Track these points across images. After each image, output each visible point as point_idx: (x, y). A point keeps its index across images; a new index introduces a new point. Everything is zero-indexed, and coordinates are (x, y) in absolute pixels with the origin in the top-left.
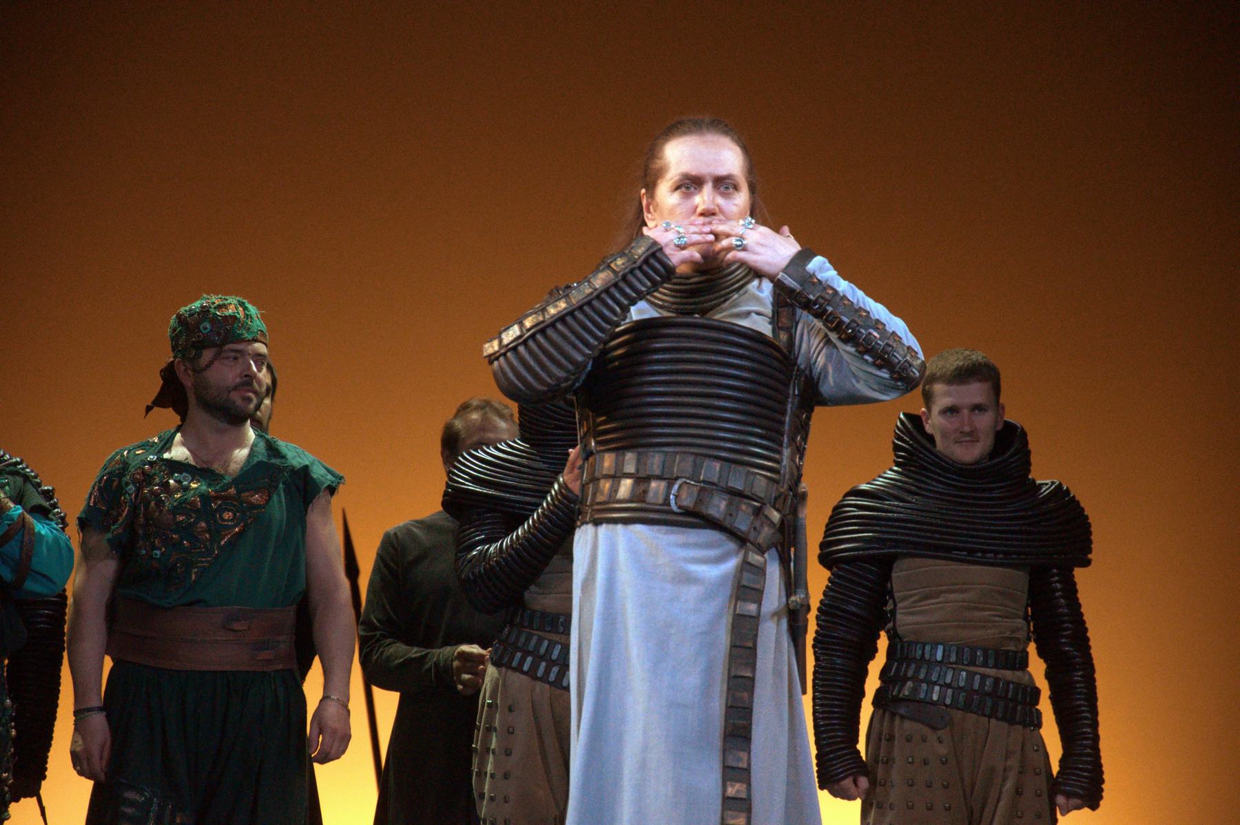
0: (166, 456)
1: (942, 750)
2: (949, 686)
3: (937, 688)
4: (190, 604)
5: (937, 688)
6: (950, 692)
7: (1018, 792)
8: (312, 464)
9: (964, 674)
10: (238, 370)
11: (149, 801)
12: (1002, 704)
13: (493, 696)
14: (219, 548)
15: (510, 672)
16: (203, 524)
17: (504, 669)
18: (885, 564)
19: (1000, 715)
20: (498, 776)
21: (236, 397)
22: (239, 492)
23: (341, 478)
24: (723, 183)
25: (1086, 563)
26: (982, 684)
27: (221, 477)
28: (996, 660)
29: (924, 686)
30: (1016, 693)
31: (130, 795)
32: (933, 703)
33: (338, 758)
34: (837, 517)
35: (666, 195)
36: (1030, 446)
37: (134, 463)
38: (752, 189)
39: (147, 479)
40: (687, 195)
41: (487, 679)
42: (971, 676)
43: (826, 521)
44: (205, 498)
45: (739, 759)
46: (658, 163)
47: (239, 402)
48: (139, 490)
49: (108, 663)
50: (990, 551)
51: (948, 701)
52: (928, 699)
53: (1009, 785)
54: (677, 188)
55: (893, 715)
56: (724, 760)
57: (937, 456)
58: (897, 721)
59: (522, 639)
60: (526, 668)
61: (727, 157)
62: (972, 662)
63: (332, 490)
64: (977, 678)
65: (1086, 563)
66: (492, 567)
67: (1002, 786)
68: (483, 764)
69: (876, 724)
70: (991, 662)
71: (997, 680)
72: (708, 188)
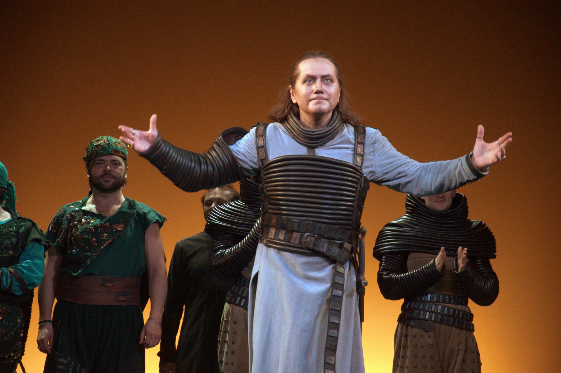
0: (83, 208)
1: (430, 341)
2: (433, 312)
3: (428, 313)
4: (88, 275)
5: (428, 313)
6: (434, 314)
7: (464, 360)
8: (149, 212)
9: (440, 307)
10: (102, 169)
11: (70, 363)
12: (457, 320)
13: (227, 316)
14: (101, 250)
15: (235, 306)
16: (95, 239)
17: (232, 305)
18: (405, 255)
19: (456, 325)
20: (229, 353)
21: (101, 180)
22: (110, 225)
23: (164, 219)
24: (325, 79)
25: (494, 257)
26: (448, 311)
27: (105, 217)
28: (455, 300)
29: (422, 312)
30: (463, 316)
31: (61, 360)
32: (426, 320)
33: (153, 346)
34: (381, 235)
35: (301, 88)
36: (468, 204)
37: (68, 211)
38: (340, 83)
39: (72, 218)
40: (309, 85)
41: (225, 309)
42: (443, 307)
43: (376, 238)
44: (96, 227)
45: (331, 360)
46: (296, 72)
47: (103, 183)
48: (69, 223)
49: (56, 301)
50: (452, 250)
51: (433, 319)
52: (424, 318)
53: (460, 357)
54: (304, 82)
55: (408, 325)
56: (325, 360)
57: (425, 207)
58: (410, 327)
59: (240, 291)
60: (242, 304)
61: (326, 67)
62: (444, 302)
63: (160, 224)
64: (446, 309)
65: (494, 257)
66: (226, 260)
67: (457, 357)
68: (222, 347)
69: (399, 329)
70: (452, 301)
71: (455, 310)
72: (318, 81)
